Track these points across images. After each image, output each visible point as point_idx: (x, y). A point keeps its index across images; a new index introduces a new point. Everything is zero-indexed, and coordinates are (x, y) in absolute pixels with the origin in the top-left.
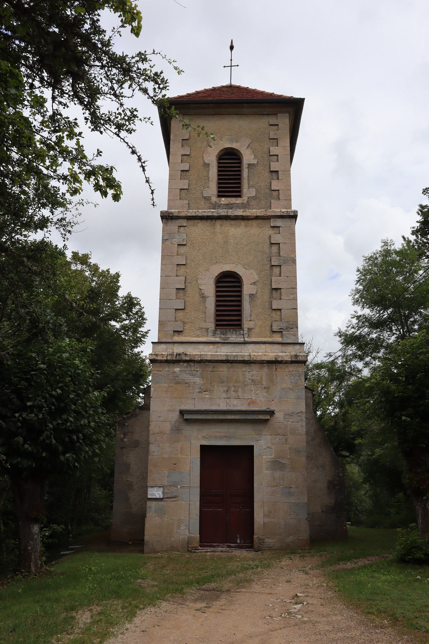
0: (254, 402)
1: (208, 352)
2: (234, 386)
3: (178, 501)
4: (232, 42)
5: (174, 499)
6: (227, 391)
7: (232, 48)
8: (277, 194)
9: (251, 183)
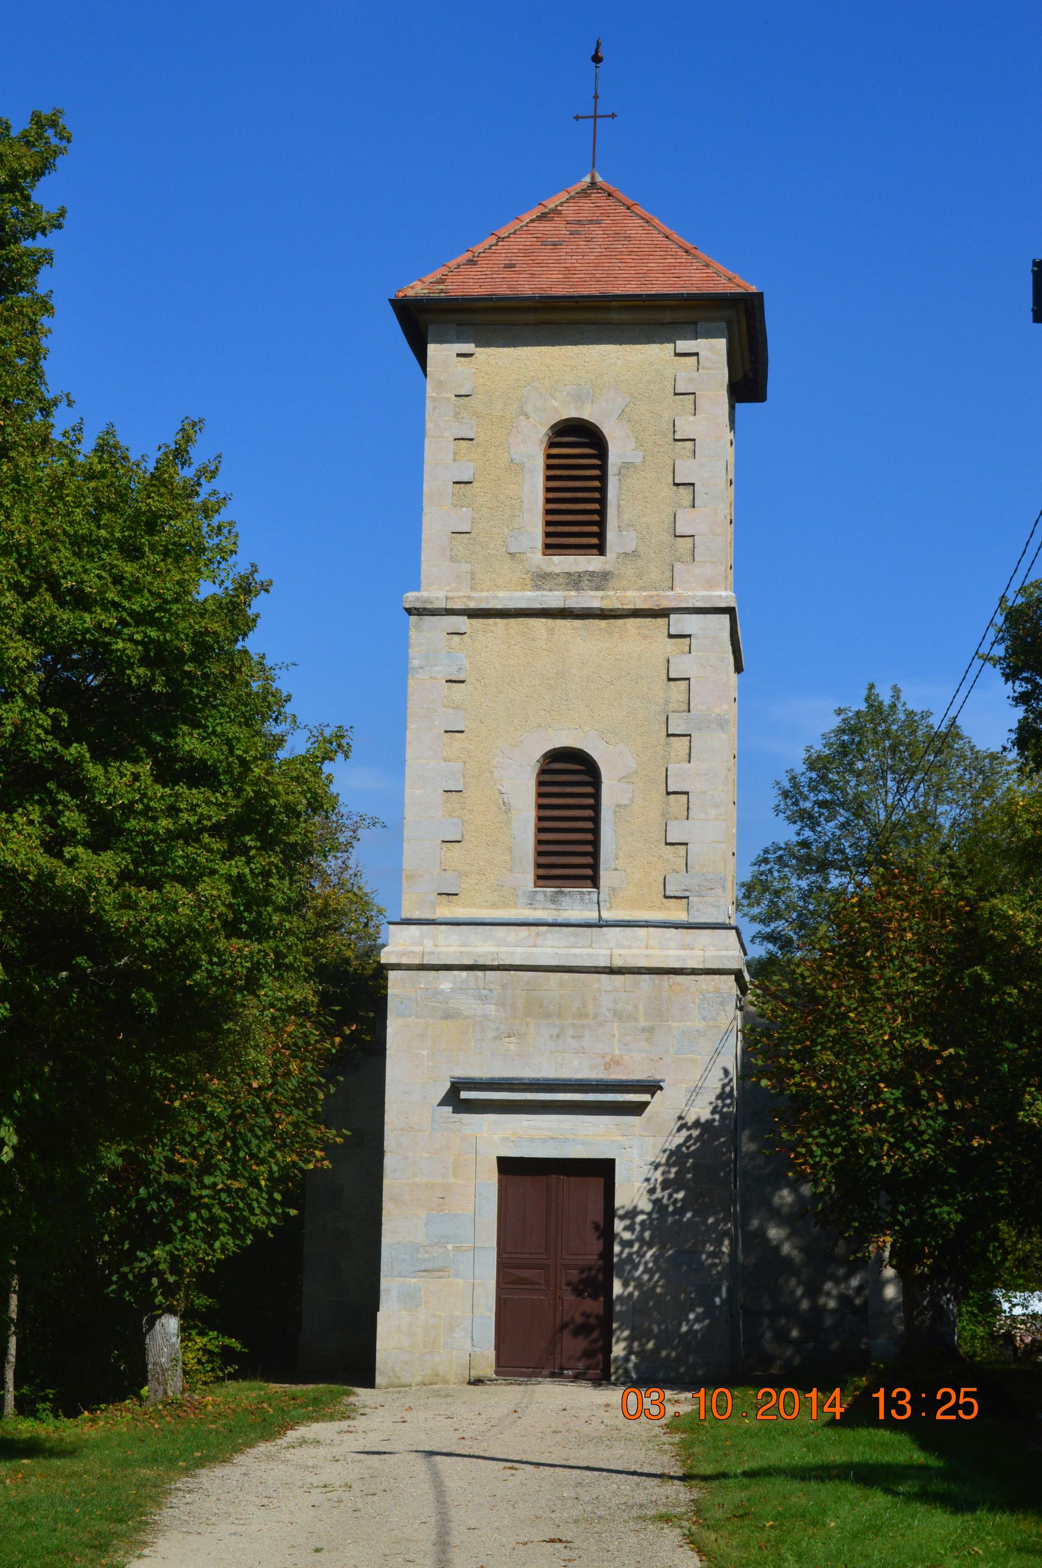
0: (617, 1063)
1: (514, 947)
2: (574, 1025)
3: (449, 1277)
4: (598, 44)
5: (440, 1273)
6: (558, 1036)
7: (597, 59)
8: (690, 546)
9: (626, 517)
